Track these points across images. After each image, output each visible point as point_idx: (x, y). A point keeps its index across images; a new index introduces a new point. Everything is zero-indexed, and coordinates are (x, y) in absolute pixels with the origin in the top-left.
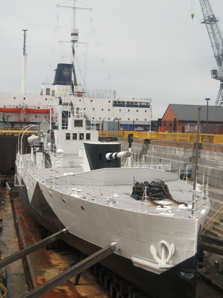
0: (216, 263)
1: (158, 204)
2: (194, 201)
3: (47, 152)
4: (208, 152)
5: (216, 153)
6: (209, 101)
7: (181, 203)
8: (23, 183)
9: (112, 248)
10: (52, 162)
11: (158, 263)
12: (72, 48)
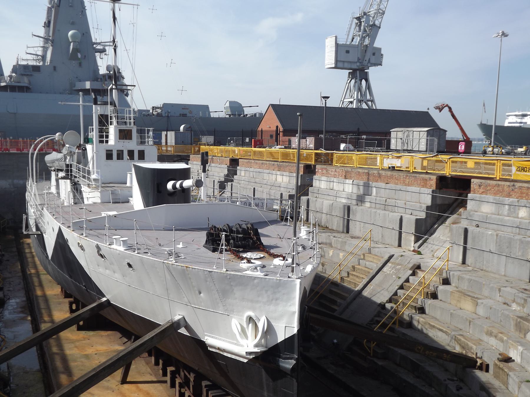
0: (334, 343)
1: (242, 259)
2: (294, 254)
3: (76, 180)
4: (324, 178)
8: (38, 229)
9: (175, 325)
10: (85, 195)
11: (242, 346)
12: (112, 12)
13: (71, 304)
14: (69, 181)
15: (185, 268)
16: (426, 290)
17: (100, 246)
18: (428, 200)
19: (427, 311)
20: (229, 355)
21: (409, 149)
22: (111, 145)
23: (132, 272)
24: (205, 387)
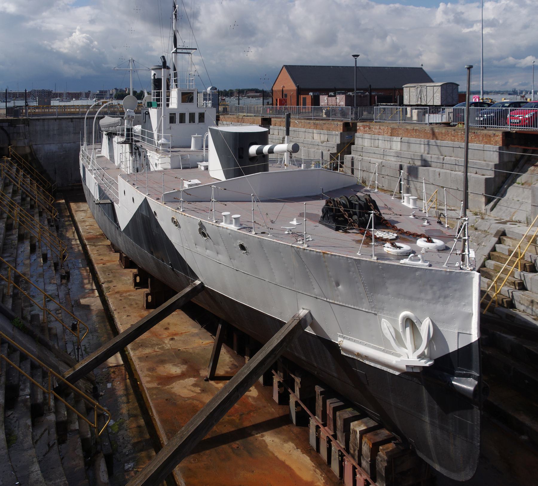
4: (367, 136)
5: (380, 137)
6: (358, 58)
7: (421, 236)
13: (135, 276)
14: (128, 145)
15: (322, 254)
16: (523, 262)
17: (204, 224)
18: (495, 159)
19: (528, 286)
20: (372, 364)
21: (423, 104)
22: (174, 109)
23: (245, 255)
24: (321, 395)
